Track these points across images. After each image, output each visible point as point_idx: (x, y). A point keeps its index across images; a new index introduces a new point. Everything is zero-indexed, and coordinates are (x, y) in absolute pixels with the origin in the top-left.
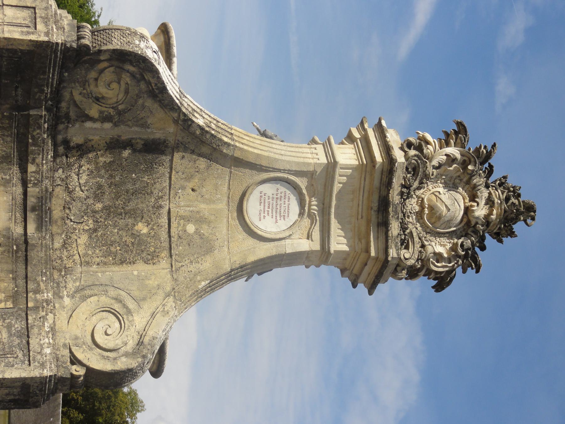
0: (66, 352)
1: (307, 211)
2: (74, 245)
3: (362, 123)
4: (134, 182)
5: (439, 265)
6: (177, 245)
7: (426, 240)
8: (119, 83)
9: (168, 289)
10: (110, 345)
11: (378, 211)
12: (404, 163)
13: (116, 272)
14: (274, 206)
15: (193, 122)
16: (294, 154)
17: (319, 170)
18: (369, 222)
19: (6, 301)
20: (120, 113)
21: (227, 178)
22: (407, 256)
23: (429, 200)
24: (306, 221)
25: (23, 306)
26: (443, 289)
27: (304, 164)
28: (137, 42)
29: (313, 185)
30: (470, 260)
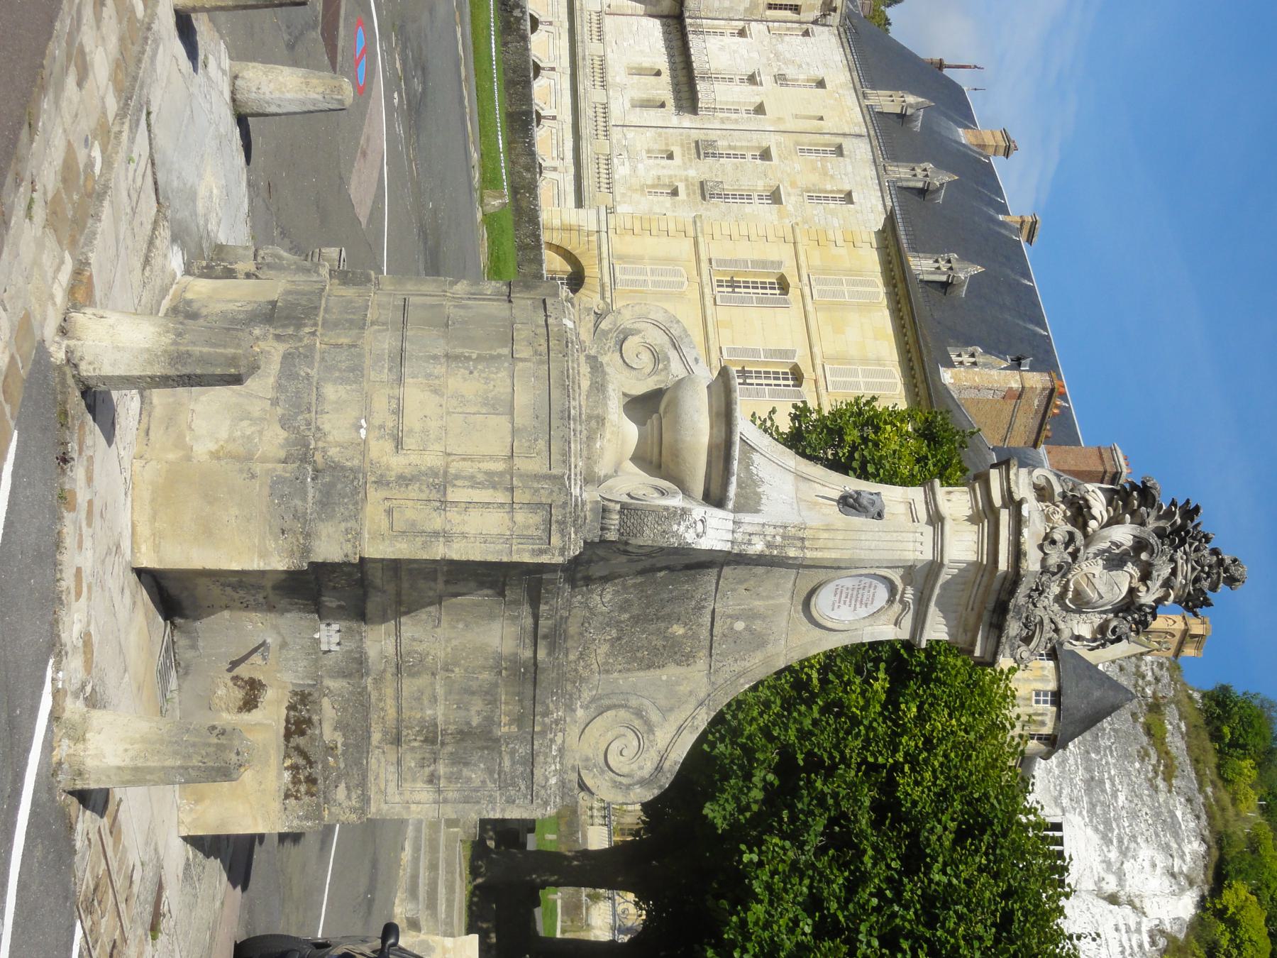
0: (574, 777)
4: (671, 592)
9: (702, 695)
11: (994, 611)
17: (919, 565)
18: (979, 617)
19: (510, 725)
24: (897, 607)
25: (529, 729)
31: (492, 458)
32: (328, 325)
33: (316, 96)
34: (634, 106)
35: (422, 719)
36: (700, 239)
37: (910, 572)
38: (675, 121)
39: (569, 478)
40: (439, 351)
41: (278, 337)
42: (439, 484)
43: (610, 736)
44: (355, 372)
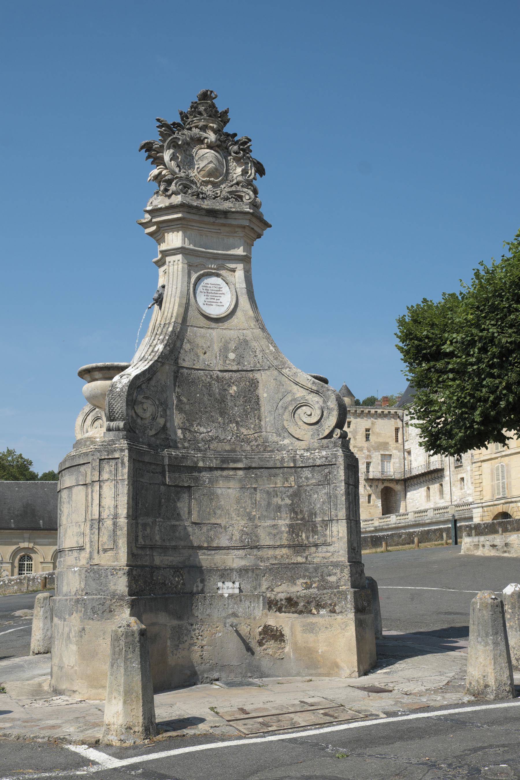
1: (215, 271)
2: (248, 437)
3: (141, 224)
5: (250, 172)
6: (244, 366)
7: (233, 181)
8: (143, 403)
9: (276, 373)
10: (319, 412)
12: (182, 196)
13: (265, 408)
14: (213, 295)
15: (162, 351)
16: (175, 278)
18: (224, 225)
20: (161, 404)
21: (195, 328)
22: (247, 197)
23: (203, 176)
26: (264, 170)
27: (183, 271)
28: (118, 390)
29: (197, 266)
30: (245, 146)
33: (42, 611)
34: (443, 498)
35: (288, 532)
36: (482, 459)
37: (191, 267)
38: (447, 479)
43: (300, 423)
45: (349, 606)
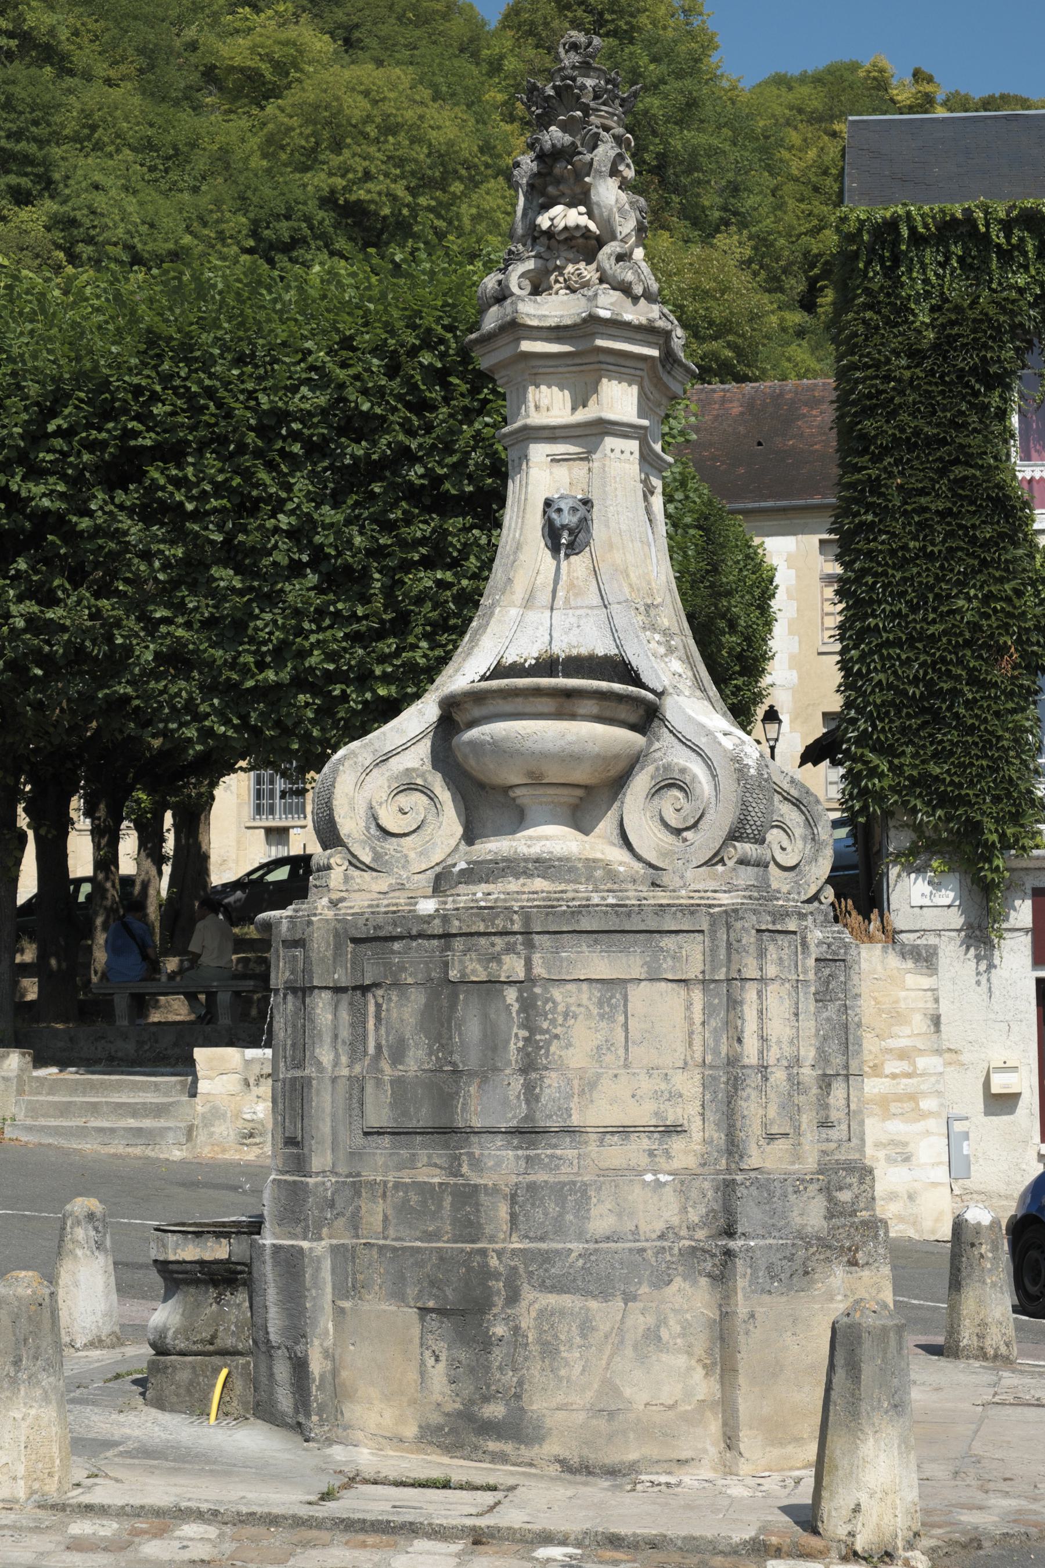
31: (689, 1006)
32: (470, 1228)
39: (710, 906)
40: (517, 1083)
41: (513, 1298)
42: (729, 1082)
44: (575, 1195)
45: (881, 1251)
